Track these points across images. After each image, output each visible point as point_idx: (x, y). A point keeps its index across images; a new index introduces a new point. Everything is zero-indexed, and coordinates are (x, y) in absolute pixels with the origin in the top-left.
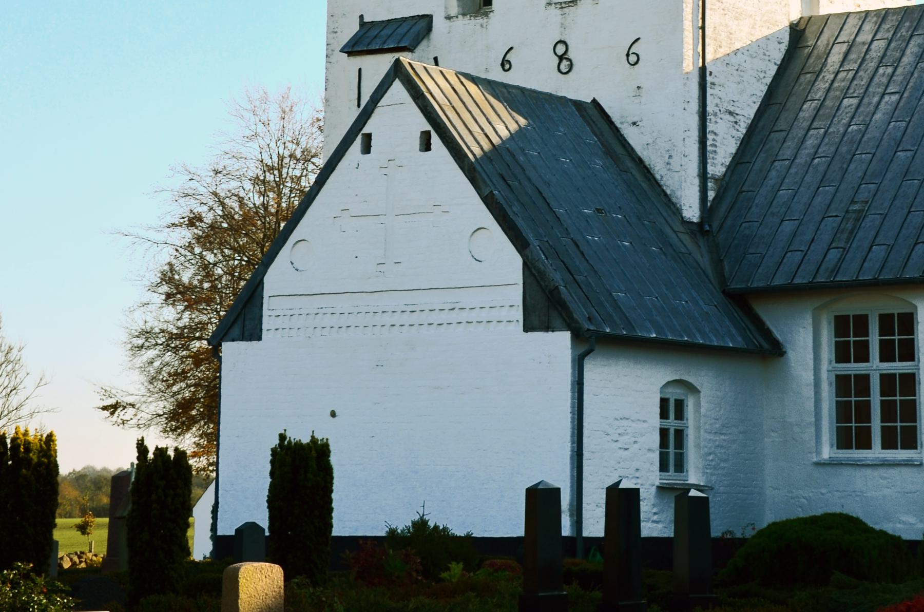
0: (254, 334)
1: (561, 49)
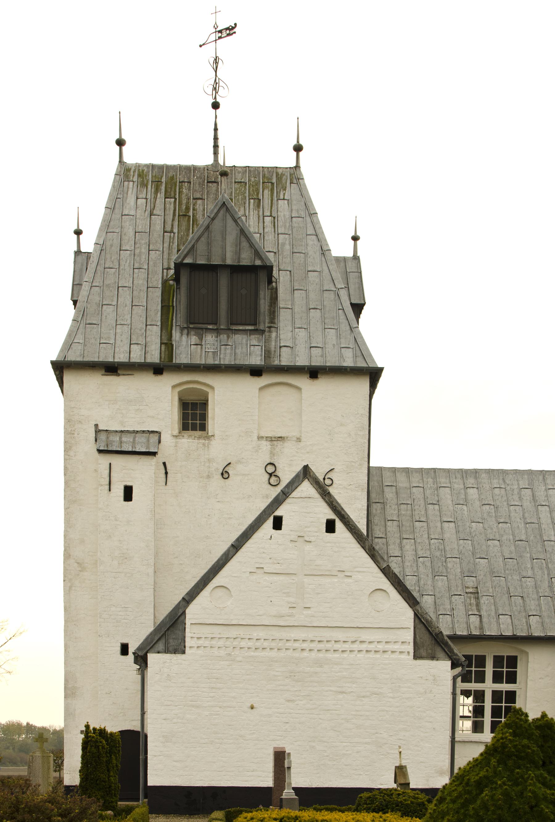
0: (180, 649)
1: (270, 469)
